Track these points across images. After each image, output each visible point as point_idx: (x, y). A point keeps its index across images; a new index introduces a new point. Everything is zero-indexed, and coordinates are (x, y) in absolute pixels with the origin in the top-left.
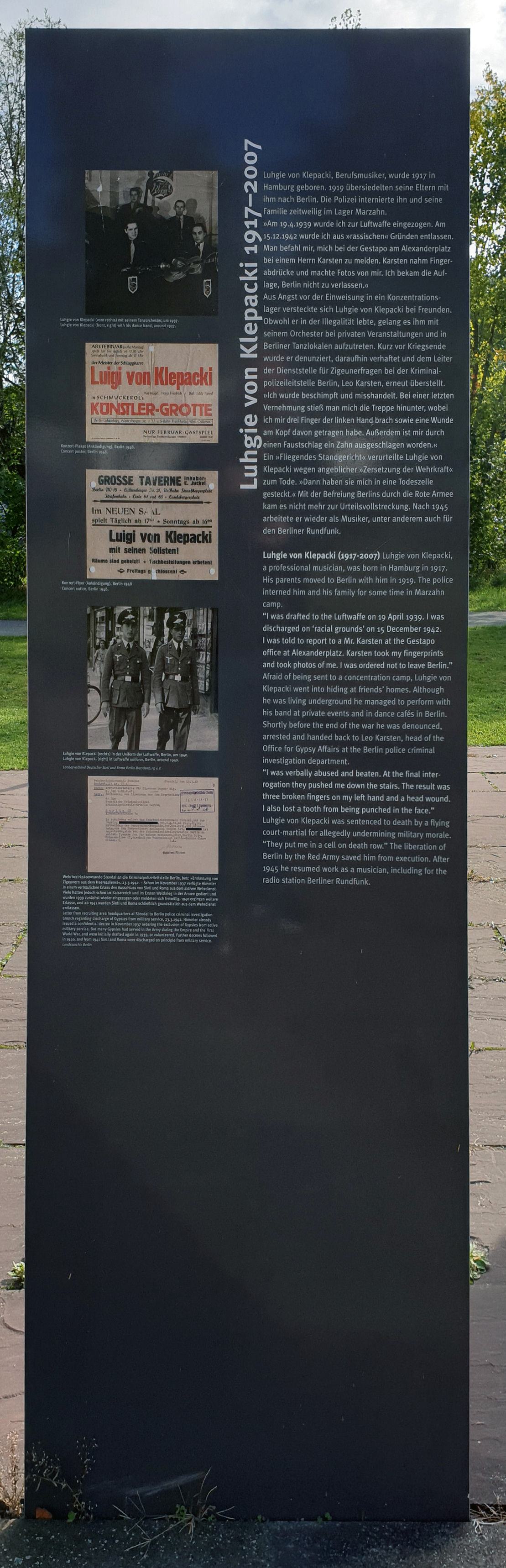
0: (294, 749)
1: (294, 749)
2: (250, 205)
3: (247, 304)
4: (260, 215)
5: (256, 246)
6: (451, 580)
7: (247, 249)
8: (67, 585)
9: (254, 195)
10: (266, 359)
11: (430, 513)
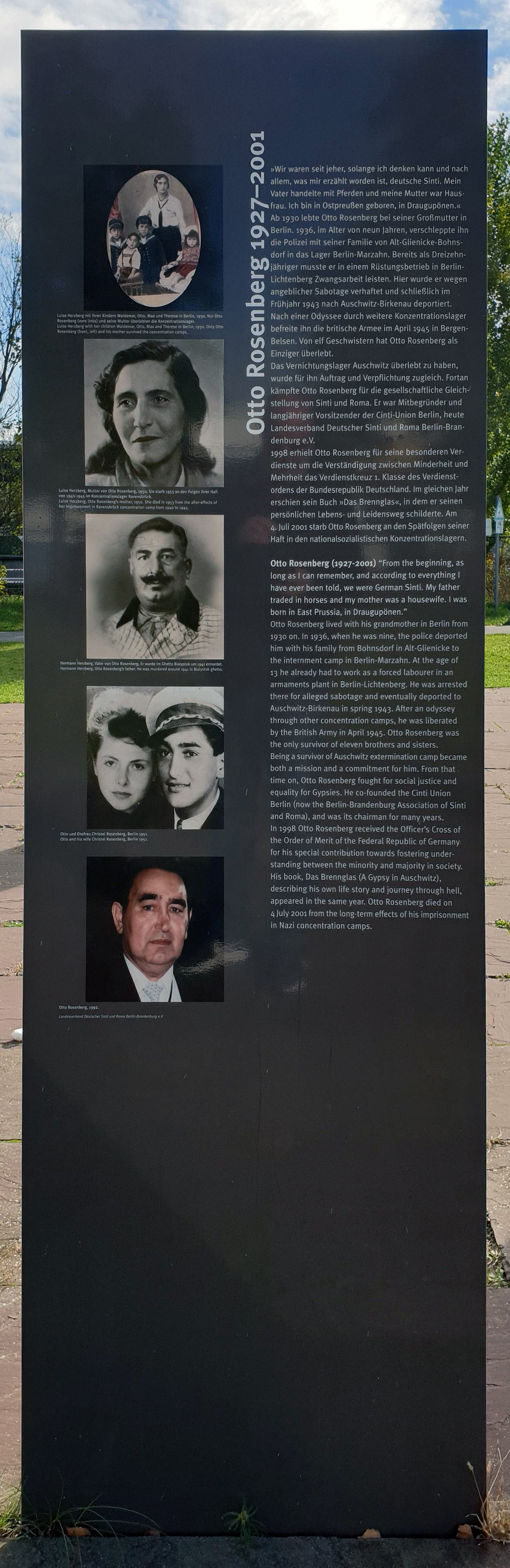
0: (311, 793)
1: (311, 793)
2: (257, 196)
3: (262, 283)
4: (267, 206)
5: (263, 241)
7: (254, 245)
8: (66, 666)
10: (273, 379)
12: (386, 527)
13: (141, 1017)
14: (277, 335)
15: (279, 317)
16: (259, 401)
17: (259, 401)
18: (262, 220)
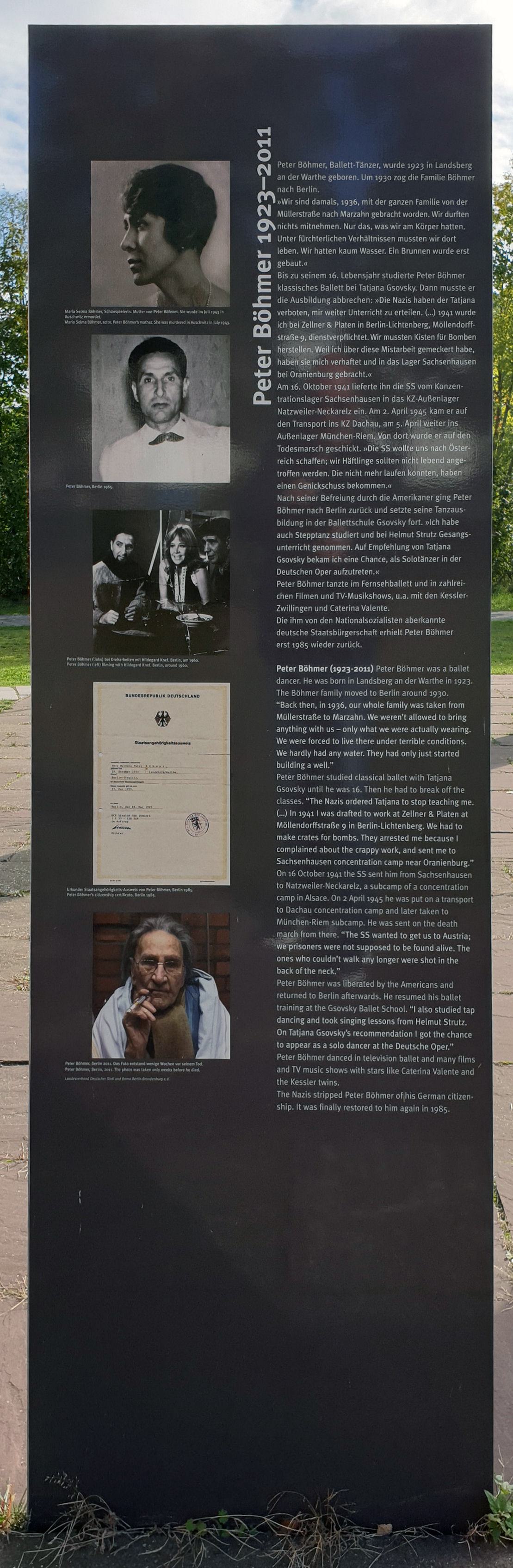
3: (269, 262)
5: (270, 235)
6: (470, 1035)
7: (260, 238)
9: (267, 178)
11: (440, 245)
12: (397, 682)
13: (147, 1079)
14: (285, 269)
15: (288, 706)
16: (266, 370)
17: (266, 370)
18: (269, 214)
